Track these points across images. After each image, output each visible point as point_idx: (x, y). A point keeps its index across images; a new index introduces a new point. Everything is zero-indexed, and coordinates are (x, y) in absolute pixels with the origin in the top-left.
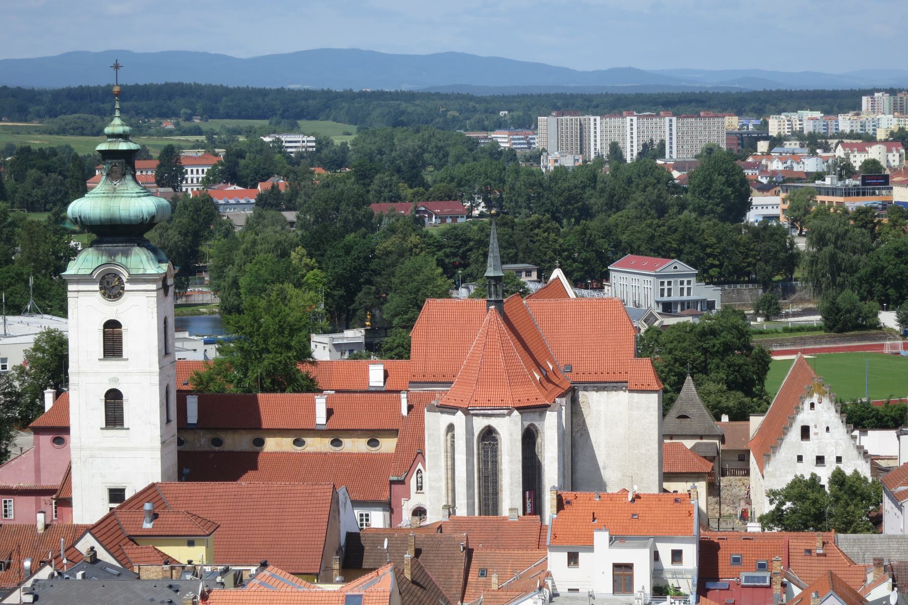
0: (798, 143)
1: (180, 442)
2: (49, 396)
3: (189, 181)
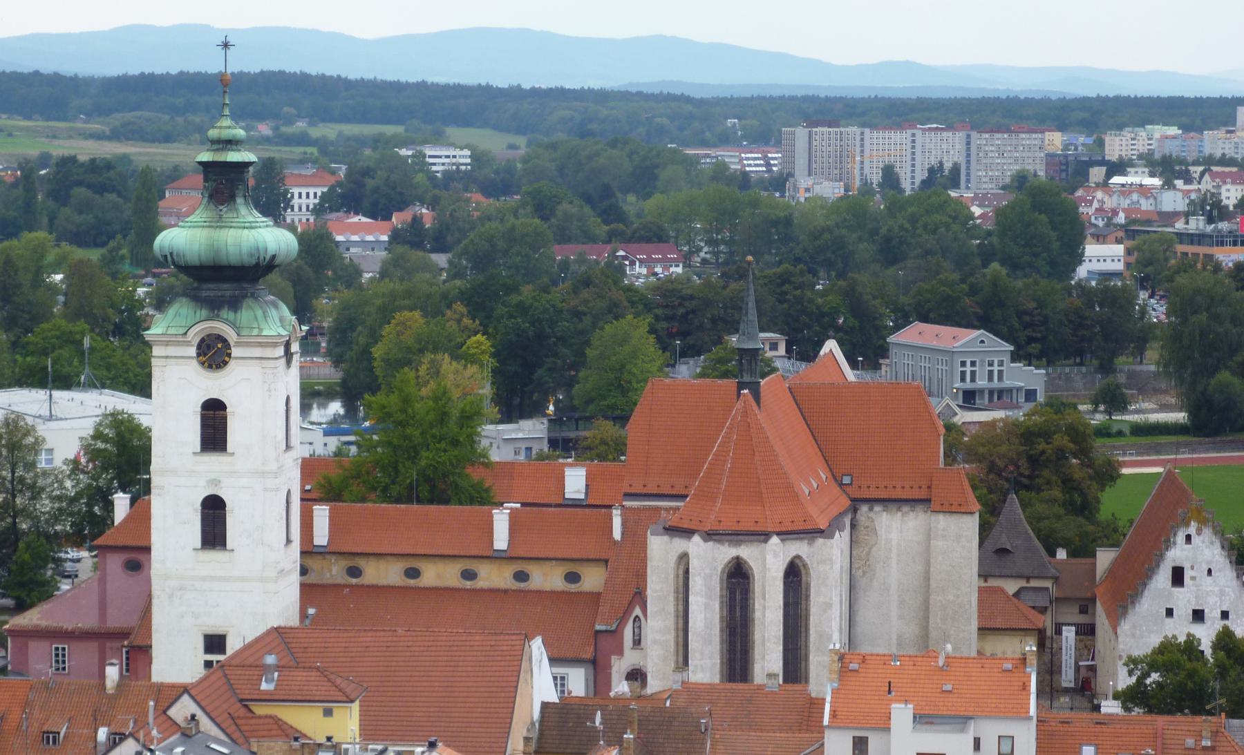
0: (1147, 170)
1: (304, 571)
2: (121, 503)
3: (296, 209)
